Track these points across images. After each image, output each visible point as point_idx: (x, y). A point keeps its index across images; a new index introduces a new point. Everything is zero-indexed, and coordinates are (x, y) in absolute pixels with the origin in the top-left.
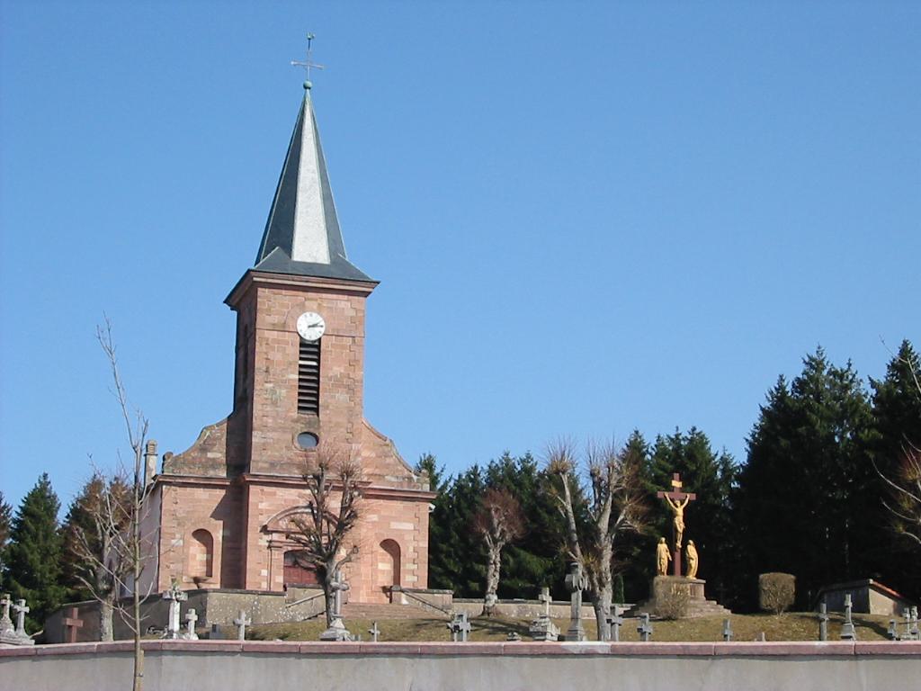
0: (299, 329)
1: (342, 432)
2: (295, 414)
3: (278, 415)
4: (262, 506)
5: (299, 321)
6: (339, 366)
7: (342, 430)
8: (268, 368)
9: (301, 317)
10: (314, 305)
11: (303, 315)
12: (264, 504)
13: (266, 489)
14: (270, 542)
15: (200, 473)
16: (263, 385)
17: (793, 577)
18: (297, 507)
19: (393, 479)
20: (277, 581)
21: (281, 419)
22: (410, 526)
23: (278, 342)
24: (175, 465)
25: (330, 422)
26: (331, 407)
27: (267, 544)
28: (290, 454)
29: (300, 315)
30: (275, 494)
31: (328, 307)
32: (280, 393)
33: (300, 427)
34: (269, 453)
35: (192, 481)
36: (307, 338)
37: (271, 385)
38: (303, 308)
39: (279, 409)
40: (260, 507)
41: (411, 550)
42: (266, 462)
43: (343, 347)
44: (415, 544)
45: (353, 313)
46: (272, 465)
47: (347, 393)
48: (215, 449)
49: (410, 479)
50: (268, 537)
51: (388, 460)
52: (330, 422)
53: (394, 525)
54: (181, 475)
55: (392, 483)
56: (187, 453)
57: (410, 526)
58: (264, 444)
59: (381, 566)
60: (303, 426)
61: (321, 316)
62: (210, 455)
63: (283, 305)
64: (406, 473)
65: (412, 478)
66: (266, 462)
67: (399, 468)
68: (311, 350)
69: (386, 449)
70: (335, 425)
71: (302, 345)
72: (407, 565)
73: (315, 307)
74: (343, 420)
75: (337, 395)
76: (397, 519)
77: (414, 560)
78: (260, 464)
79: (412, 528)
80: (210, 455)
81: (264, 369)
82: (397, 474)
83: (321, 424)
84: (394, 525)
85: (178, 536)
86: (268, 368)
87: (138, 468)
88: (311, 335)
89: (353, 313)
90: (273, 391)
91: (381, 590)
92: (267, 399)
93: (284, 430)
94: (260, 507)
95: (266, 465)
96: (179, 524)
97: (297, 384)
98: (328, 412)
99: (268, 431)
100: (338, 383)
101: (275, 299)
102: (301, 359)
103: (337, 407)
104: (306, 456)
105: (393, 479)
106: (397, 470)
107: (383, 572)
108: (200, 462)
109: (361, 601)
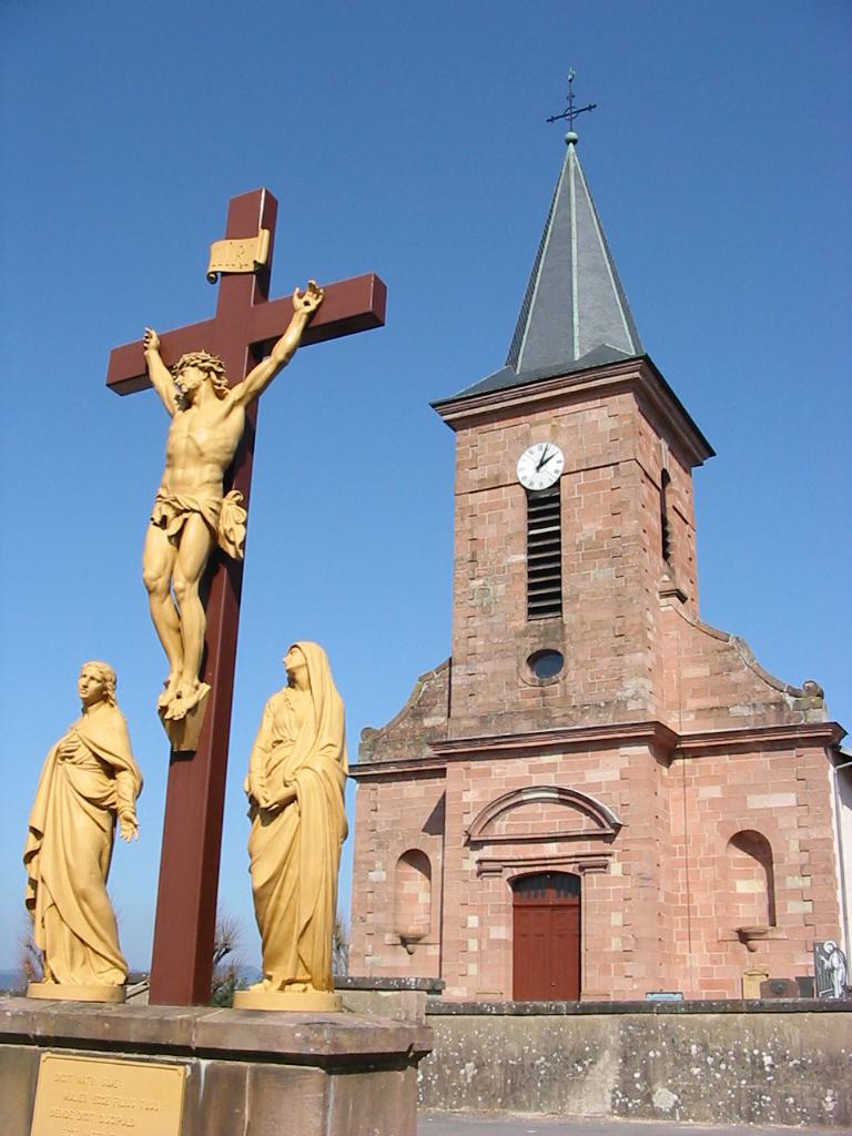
0: (520, 475)
1: (606, 638)
2: (521, 621)
3: (492, 631)
4: (468, 797)
5: (521, 464)
6: (594, 521)
7: (605, 633)
8: (474, 554)
9: (523, 457)
10: (545, 430)
11: (527, 452)
12: (470, 794)
13: (474, 765)
14: (480, 862)
15: (411, 754)
16: (467, 585)
17: (631, 394)
18: (519, 791)
19: (746, 712)
20: (493, 935)
21: (498, 636)
22: (790, 799)
23: (490, 507)
24: (374, 749)
25: (583, 623)
26: (581, 597)
27: (475, 867)
28: (516, 695)
29: (522, 453)
30: (488, 772)
31: (570, 428)
32: (495, 592)
33: (530, 645)
34: (480, 700)
35: (393, 769)
36: (536, 487)
37: (481, 582)
38: (526, 441)
39: (494, 620)
40: (464, 800)
41: (794, 847)
42: (474, 717)
43: (599, 486)
44: (801, 834)
45: (612, 424)
46: (484, 720)
47: (611, 565)
48: (435, 711)
49: (780, 704)
50: (477, 855)
51: (734, 677)
52: (583, 623)
53: (756, 802)
54: (384, 761)
55: (745, 719)
56: (392, 725)
57: (790, 799)
58: (471, 686)
59: (742, 887)
60: (537, 640)
61: (557, 445)
62: (428, 722)
63: (495, 447)
64: (773, 695)
65: (784, 702)
66: (474, 717)
67: (758, 688)
68: (544, 506)
69: (729, 656)
70: (593, 629)
71: (531, 503)
72: (789, 879)
73: (547, 433)
74: (605, 615)
75: (592, 572)
76: (761, 790)
77: (802, 867)
78: (465, 723)
79: (794, 803)
80: (428, 722)
81: (468, 556)
82: (754, 700)
83: (567, 631)
84: (756, 802)
85: (379, 865)
86: (474, 554)
87: (91, 750)
88: (541, 481)
89: (612, 424)
90: (484, 590)
91: (736, 936)
92: (475, 607)
93: (502, 653)
94: (464, 800)
95: (473, 723)
96: (380, 845)
97: (524, 570)
98: (578, 606)
99: (479, 661)
100: (593, 551)
101: (484, 441)
102: (531, 527)
103: (594, 594)
104: (543, 694)
105: (746, 712)
106: (755, 692)
107: (750, 898)
108: (413, 737)
109: (38, 1033)
